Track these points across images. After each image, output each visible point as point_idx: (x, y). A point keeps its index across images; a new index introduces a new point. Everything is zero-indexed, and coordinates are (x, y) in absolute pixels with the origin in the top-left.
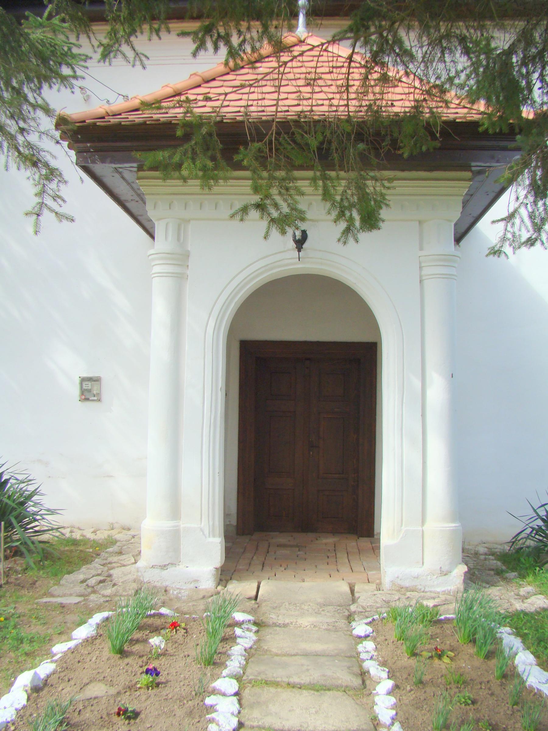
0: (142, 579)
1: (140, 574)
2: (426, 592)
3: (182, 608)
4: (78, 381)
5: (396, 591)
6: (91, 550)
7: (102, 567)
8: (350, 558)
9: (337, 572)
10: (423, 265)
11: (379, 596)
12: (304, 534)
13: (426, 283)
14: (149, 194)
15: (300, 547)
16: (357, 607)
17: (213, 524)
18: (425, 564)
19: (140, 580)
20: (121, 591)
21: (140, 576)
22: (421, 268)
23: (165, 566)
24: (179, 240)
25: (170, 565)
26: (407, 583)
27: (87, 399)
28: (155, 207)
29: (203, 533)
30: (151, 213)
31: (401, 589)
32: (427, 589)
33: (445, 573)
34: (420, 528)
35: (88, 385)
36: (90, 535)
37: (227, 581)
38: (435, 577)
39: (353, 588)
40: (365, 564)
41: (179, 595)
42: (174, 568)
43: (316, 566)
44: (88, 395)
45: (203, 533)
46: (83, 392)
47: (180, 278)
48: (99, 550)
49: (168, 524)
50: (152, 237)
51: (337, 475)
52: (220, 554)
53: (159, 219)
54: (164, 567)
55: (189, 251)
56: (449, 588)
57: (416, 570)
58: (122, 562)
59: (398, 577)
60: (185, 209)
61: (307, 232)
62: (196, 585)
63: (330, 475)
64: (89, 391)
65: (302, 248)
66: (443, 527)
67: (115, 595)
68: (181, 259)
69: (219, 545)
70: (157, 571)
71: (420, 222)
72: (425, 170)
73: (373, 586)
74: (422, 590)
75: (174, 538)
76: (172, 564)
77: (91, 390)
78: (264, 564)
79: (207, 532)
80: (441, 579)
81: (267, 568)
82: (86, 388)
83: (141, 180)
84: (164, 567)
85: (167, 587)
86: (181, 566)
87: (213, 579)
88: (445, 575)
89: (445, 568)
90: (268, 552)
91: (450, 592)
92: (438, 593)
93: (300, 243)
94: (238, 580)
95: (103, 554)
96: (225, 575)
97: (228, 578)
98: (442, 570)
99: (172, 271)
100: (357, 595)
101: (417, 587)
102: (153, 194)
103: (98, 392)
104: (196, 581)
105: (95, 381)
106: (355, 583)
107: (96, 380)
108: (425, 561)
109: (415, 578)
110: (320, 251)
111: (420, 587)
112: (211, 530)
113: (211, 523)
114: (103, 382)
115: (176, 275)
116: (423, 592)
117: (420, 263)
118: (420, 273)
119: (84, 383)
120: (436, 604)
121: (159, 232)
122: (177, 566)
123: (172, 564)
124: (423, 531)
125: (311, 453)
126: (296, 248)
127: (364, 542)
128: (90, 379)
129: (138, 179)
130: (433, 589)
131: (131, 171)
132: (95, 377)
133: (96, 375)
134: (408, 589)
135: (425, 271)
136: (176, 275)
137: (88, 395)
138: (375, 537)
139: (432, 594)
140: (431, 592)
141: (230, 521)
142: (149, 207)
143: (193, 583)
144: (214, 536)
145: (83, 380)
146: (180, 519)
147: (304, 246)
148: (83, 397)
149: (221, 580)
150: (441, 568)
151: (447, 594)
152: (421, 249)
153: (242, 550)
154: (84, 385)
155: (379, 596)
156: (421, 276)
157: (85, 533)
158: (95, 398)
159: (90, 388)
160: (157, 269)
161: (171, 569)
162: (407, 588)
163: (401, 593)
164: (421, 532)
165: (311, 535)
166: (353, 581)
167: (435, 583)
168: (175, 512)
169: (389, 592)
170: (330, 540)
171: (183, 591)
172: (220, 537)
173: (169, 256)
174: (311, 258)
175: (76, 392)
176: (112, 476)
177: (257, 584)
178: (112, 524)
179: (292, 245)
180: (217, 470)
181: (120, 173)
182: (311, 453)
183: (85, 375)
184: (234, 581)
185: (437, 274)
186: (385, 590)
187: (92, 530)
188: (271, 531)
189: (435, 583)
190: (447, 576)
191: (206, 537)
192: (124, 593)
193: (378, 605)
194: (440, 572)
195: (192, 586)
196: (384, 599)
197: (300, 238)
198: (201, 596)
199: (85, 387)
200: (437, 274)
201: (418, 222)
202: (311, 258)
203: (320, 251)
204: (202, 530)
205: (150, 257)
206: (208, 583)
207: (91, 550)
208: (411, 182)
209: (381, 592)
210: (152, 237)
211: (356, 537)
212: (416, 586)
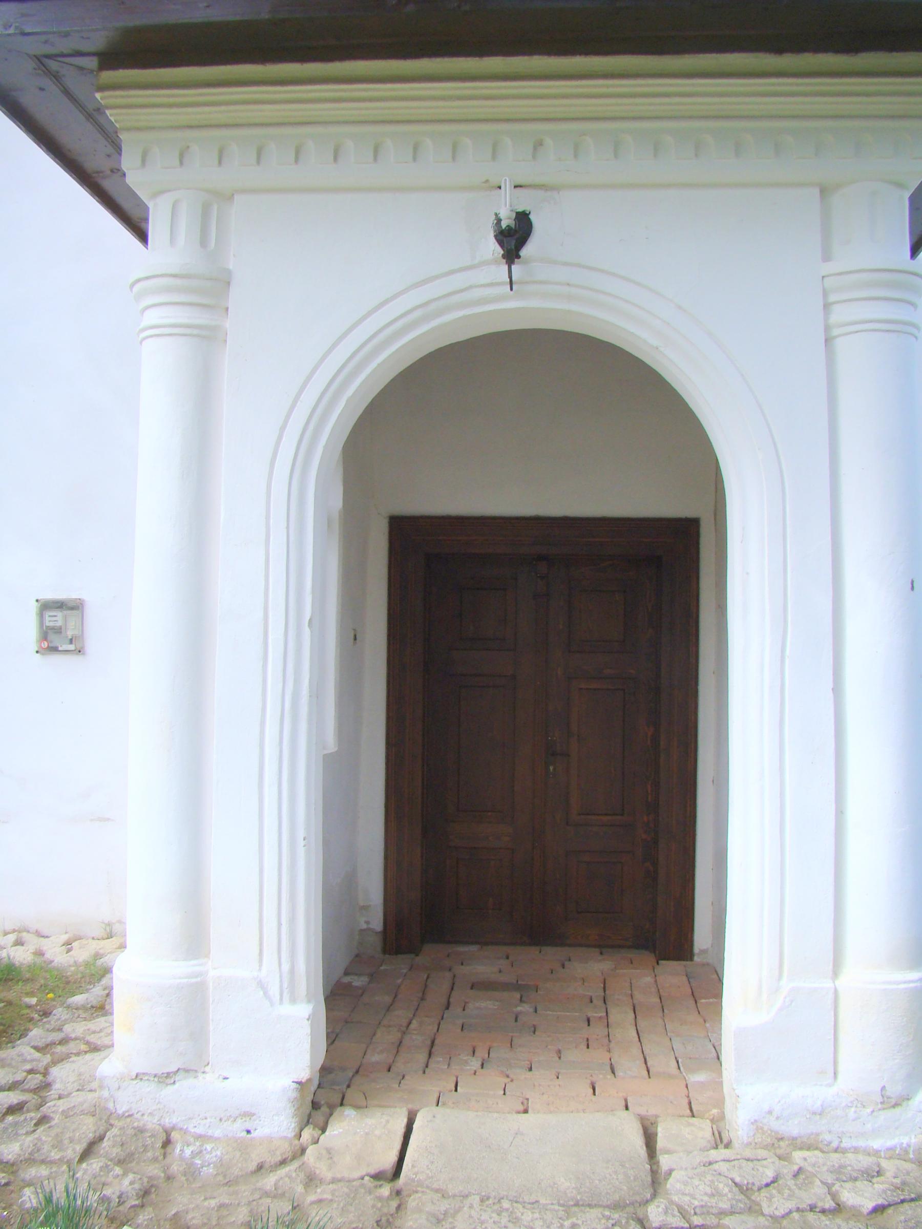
0: (111, 1105)
1: (106, 1093)
2: (844, 1151)
3: (189, 1216)
4: (34, 608)
5: (766, 1147)
6: (34, 1001)
7: (37, 1055)
8: (642, 1024)
9: (610, 1076)
10: (832, 298)
11: (723, 1167)
12: (533, 951)
13: (841, 345)
14: (128, 129)
15: (522, 989)
16: (666, 1212)
17: (292, 971)
18: (840, 1076)
19: (106, 1109)
20: (46, 1148)
21: (107, 1100)
22: (827, 307)
23: (168, 1075)
24: (204, 243)
25: (181, 1073)
26: (793, 1128)
27: (53, 649)
28: (144, 161)
29: (266, 993)
30: (137, 177)
31: (780, 1145)
32: (846, 1143)
33: (893, 1101)
34: (829, 984)
35: (55, 619)
36: (56, 955)
37: (332, 1108)
38: (869, 1110)
39: (651, 1130)
40: (677, 1044)
41: (198, 1162)
42: (191, 1081)
43: (559, 1052)
44: (56, 640)
45: (266, 993)
46: (46, 633)
47: (207, 339)
48: (53, 1000)
49: (176, 970)
50: (142, 235)
51: (609, 818)
52: (307, 1046)
53: (155, 195)
54: (166, 1078)
55: (229, 272)
56: (905, 1140)
57: (817, 1093)
58: (92, 1038)
59: (770, 1112)
60: (220, 163)
61: (531, 217)
62: (248, 1126)
63: (593, 817)
64: (58, 631)
65: (518, 257)
66: (889, 983)
67: (30, 1161)
68: (209, 289)
69: (307, 1025)
70: (147, 1088)
71: (825, 191)
72: (837, 51)
73: (702, 1130)
74: (834, 1145)
75: (192, 1009)
76: (187, 1071)
77: (60, 628)
78: (433, 1042)
79: (274, 990)
80: (884, 1116)
81: (438, 1061)
82: (51, 624)
83: (107, 93)
84: (166, 1078)
85: (173, 1128)
86: (208, 1077)
87: (290, 1111)
88: (896, 1105)
89: (895, 1090)
90: (447, 1008)
91: (906, 1152)
92: (876, 1153)
93: (514, 237)
94: (357, 1107)
95: (60, 1013)
96: (327, 1094)
97: (337, 1098)
98: (888, 1093)
99: (186, 321)
100: (665, 1161)
101: (821, 1137)
102: (139, 129)
103: (76, 632)
104: (249, 1115)
105: (72, 608)
106: (657, 1116)
107: (72, 607)
108: (841, 1068)
109: (814, 1113)
110: (566, 264)
111: (827, 1137)
112: (285, 985)
113: (286, 967)
114: (91, 612)
115: (195, 332)
116: (836, 1150)
117: (825, 294)
118: (826, 318)
119: (48, 614)
120: (880, 1201)
121: (156, 227)
122: (201, 1076)
123: (187, 1071)
124: (836, 991)
125: (551, 768)
126: (504, 256)
127: (671, 974)
128: (60, 605)
129: (101, 89)
130: (861, 1143)
131: (81, 69)
132: (71, 600)
133: (74, 596)
134: (799, 1144)
135: (839, 315)
136: (195, 332)
137: (56, 640)
138: (696, 958)
139: (860, 1157)
140: (856, 1150)
141: (367, 922)
142: (129, 162)
143: (239, 1121)
144: (293, 1000)
145: (46, 606)
146: (207, 956)
147: (523, 252)
148: (45, 645)
149: (315, 1105)
150: (883, 1088)
151: (900, 1157)
152: (827, 257)
153: (387, 999)
154: (47, 619)
155: (723, 1167)
156: (827, 328)
157: (45, 945)
158: (72, 647)
159: (59, 624)
160: (153, 317)
161: (184, 1084)
162: (794, 1139)
163: (779, 1152)
164: (831, 996)
165: (552, 954)
166: (652, 1111)
167: (869, 1126)
168: (194, 938)
169: (748, 1153)
170: (592, 967)
171: (209, 1147)
172: (309, 1001)
173: (178, 282)
174: (541, 282)
175: (31, 632)
176: (108, 819)
177: (405, 1120)
178: (109, 924)
179: (493, 249)
180: (301, 833)
181: (56, 77)
182: (551, 768)
183: (50, 595)
184: (349, 1112)
185: (871, 321)
186: (735, 1143)
187: (65, 938)
188: (457, 942)
189: (869, 1126)
190: (898, 1110)
191: (272, 1004)
192: (55, 1155)
193: (725, 1205)
194: (879, 1099)
195: (237, 1129)
196: (738, 1179)
197: (512, 224)
198: (252, 1166)
199: (48, 622)
200: (871, 321)
201: (816, 191)
202: (541, 282)
203: (566, 264)
204: (262, 985)
205: (137, 288)
206: (277, 1123)
207: (34, 1001)
208: (800, 81)
209: (723, 1153)
210: (142, 235)
211: (651, 958)
212: (818, 1134)
